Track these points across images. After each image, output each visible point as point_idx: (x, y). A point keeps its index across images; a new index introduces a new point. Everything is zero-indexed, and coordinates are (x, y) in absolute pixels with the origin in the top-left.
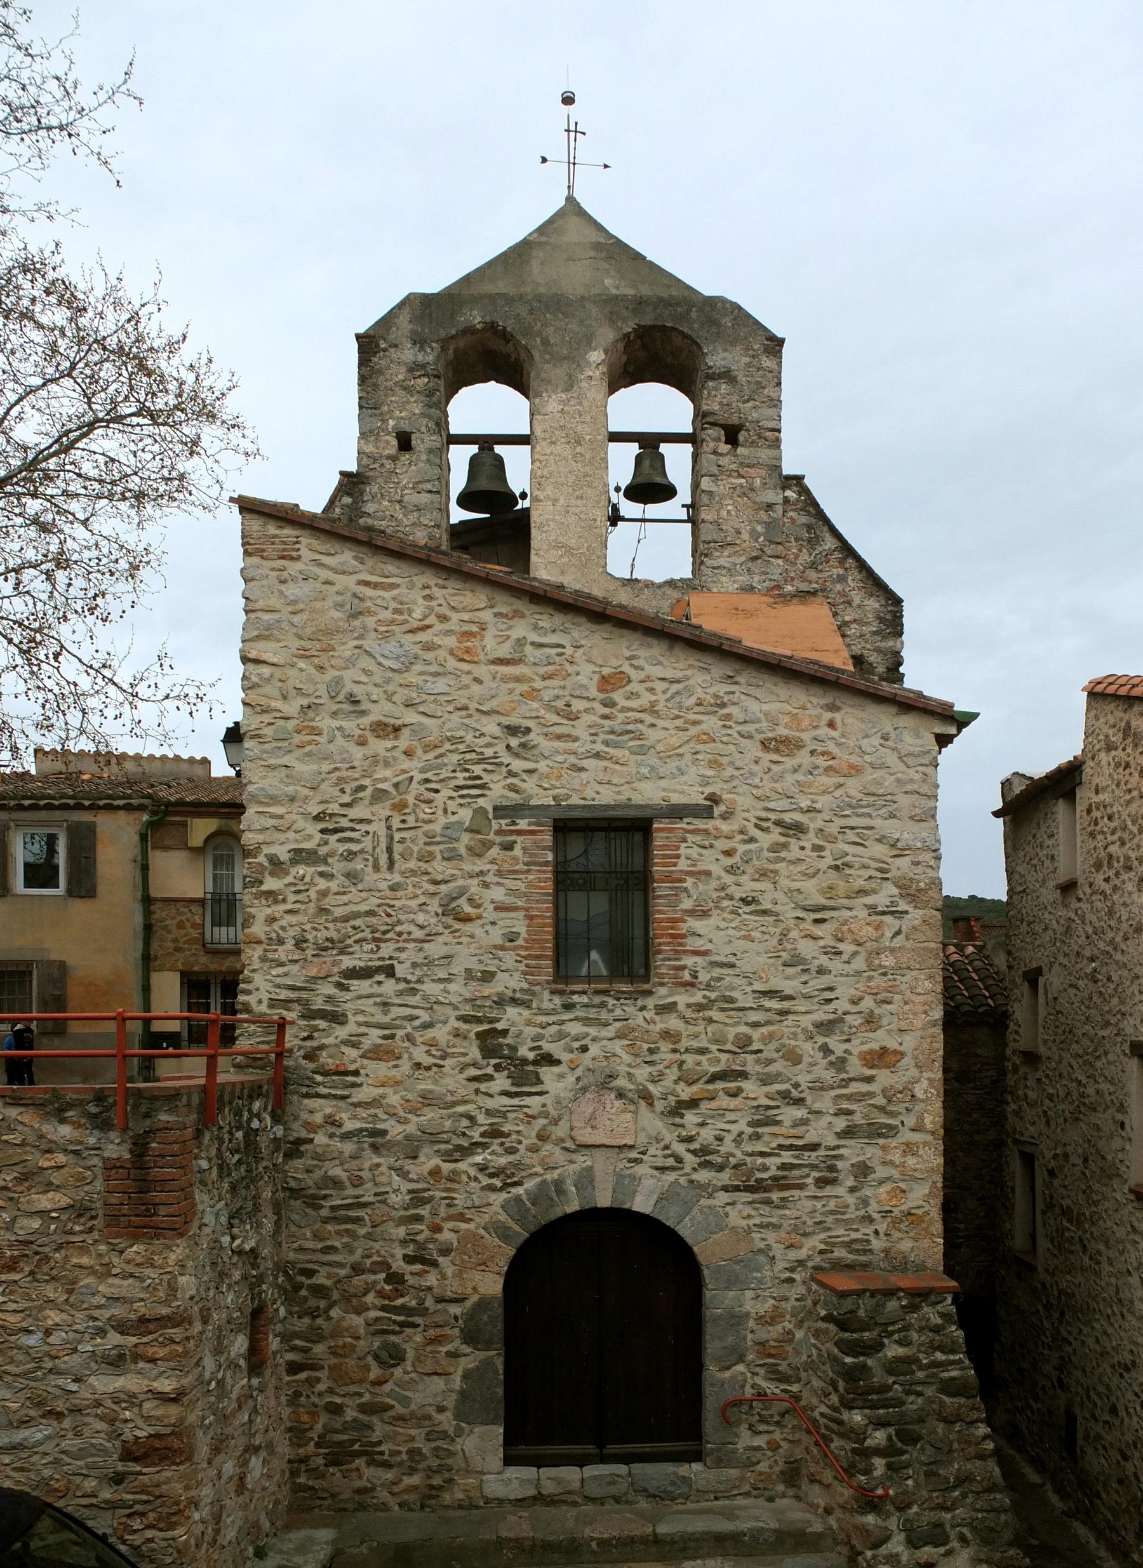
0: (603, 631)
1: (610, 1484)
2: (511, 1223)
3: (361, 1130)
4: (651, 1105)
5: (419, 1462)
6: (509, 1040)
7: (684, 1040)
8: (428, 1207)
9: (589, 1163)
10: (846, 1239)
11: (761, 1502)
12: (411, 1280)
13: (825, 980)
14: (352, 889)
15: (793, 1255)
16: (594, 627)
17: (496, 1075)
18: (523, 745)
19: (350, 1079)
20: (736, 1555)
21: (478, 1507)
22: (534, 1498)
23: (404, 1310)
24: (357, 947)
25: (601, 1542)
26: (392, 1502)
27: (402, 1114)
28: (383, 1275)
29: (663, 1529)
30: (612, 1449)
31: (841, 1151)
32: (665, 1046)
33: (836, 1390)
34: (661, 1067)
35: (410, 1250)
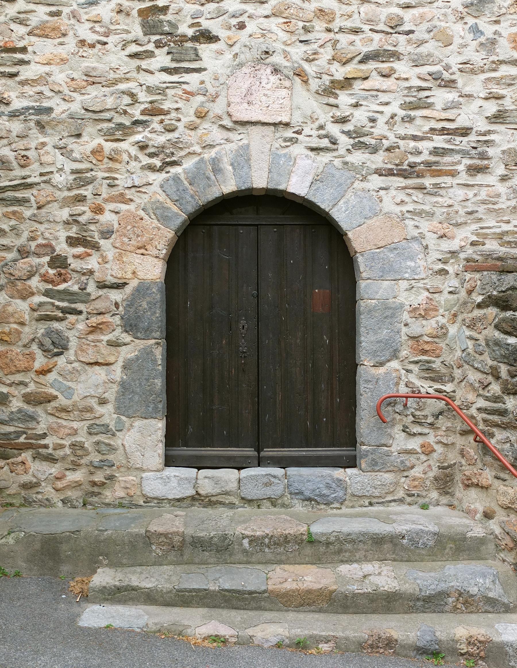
1: (266, 485)
2: (169, 204)
3: (28, 108)
4: (306, 82)
5: (81, 457)
6: (169, 17)
7: (337, 20)
8: (90, 187)
9: (245, 142)
10: (498, 231)
11: (415, 509)
12: (74, 264)
15: (446, 245)
17: (157, 51)
19: (19, 56)
20: (394, 560)
21: (137, 506)
22: (193, 498)
23: (66, 294)
25: (253, 540)
26: (56, 498)
27: (66, 91)
28: (47, 259)
29: (316, 529)
30: (268, 452)
31: (492, 137)
32: (319, 25)
33: (497, 378)
34: (315, 46)
35: (74, 231)
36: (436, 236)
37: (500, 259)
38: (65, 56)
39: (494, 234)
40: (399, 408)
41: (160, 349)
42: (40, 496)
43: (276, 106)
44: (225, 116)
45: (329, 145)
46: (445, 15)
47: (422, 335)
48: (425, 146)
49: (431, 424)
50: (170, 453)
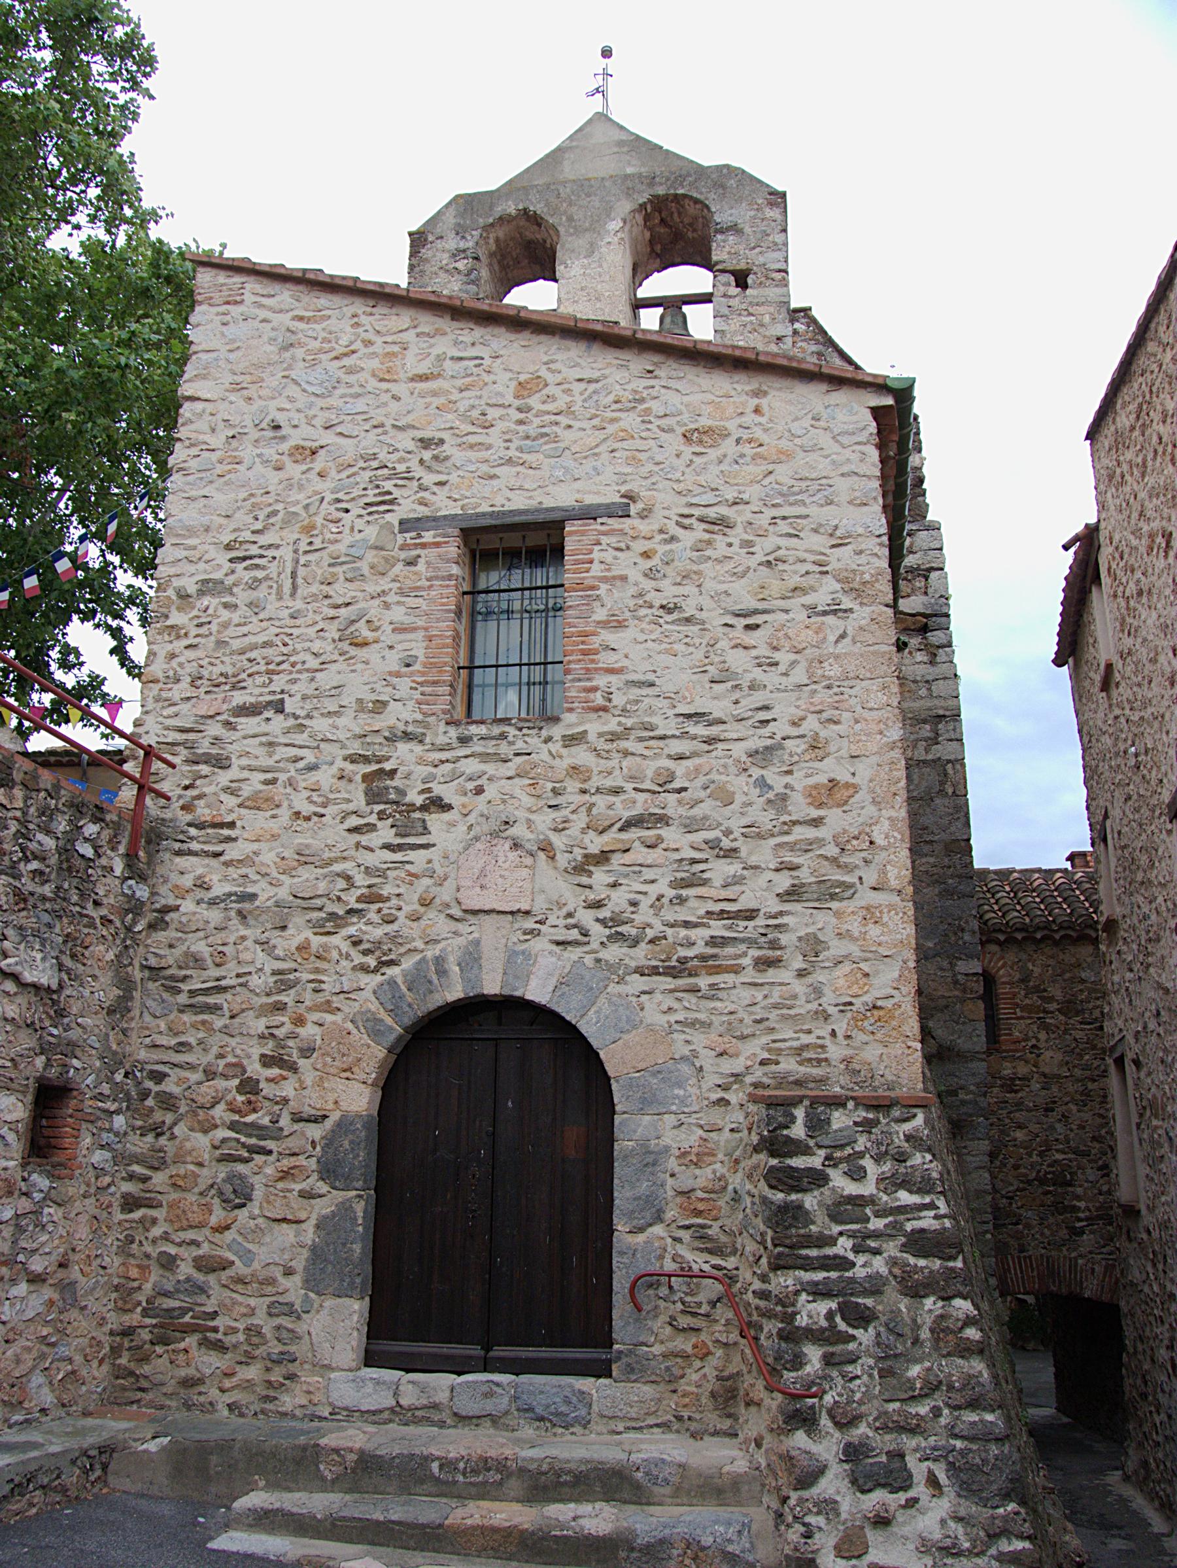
0: (525, 337)
2: (383, 1015)
3: (230, 895)
4: (553, 858)
5: (257, 1346)
6: (396, 782)
7: (595, 778)
8: (292, 991)
9: (476, 935)
10: (795, 1044)
12: (267, 1089)
13: (759, 698)
14: (254, 619)
16: (513, 336)
17: (380, 824)
18: (436, 458)
19: (226, 832)
24: (250, 681)
27: (275, 874)
28: (236, 1082)
30: (498, 1352)
32: (573, 786)
35: (268, 1048)
36: (714, 1053)
37: (798, 1083)
38: (276, 831)
39: (790, 1048)
40: (663, 1291)
41: (363, 1203)
42: (202, 1399)
43: (514, 890)
44: (453, 904)
45: (580, 937)
46: (725, 766)
47: (693, 1190)
48: (705, 933)
49: (707, 1315)
50: (371, 1347)
